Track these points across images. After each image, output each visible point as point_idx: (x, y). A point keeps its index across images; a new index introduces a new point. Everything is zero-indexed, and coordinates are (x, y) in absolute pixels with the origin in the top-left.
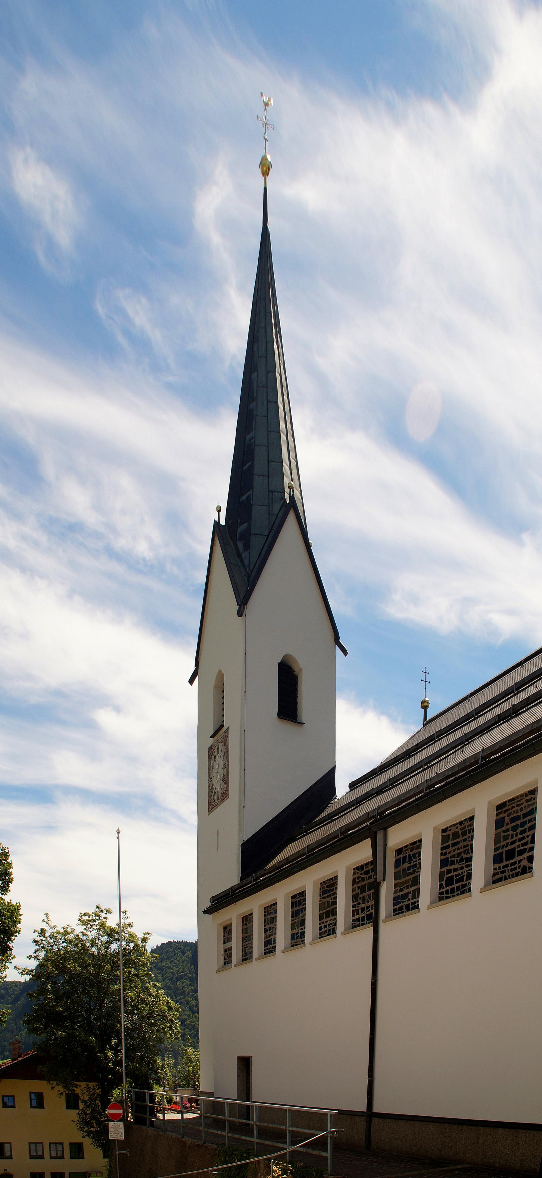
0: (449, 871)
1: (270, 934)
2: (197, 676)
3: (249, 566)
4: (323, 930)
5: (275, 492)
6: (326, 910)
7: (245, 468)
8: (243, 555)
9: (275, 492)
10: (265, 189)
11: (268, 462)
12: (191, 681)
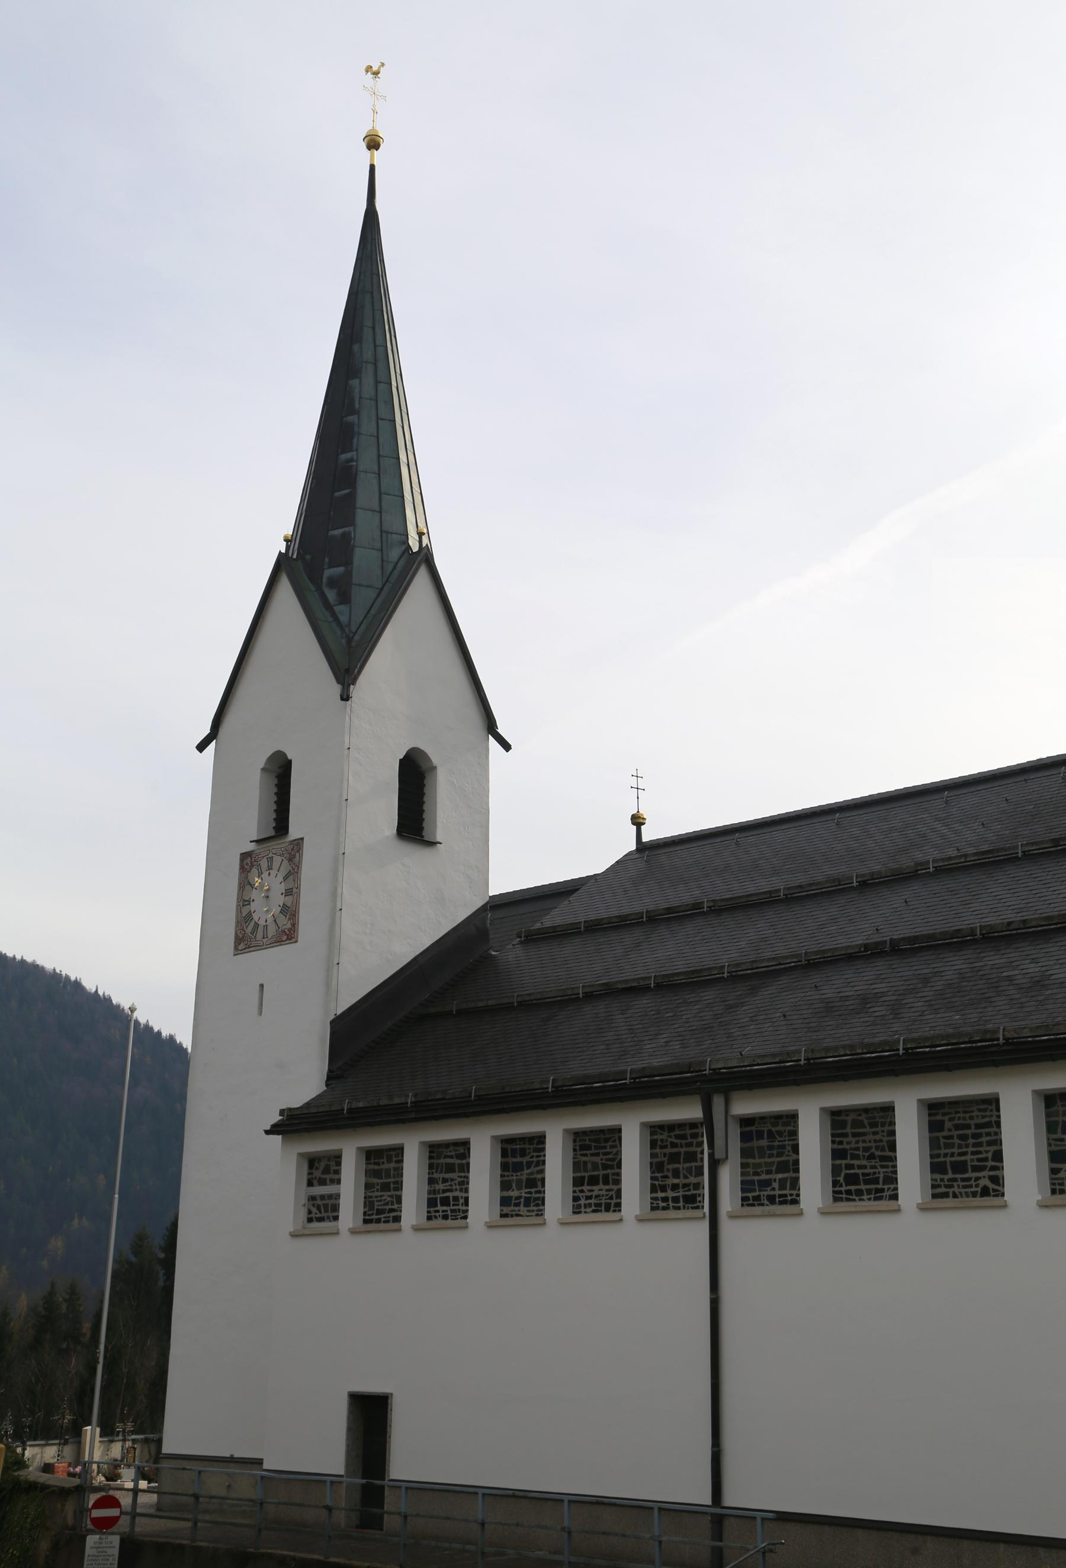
1: (445, 1188)
2: (214, 743)
3: (349, 625)
4: (582, 1202)
6: (589, 1174)
7: (337, 494)
9: (391, 533)
10: (372, 168)
11: (380, 494)
12: (201, 747)
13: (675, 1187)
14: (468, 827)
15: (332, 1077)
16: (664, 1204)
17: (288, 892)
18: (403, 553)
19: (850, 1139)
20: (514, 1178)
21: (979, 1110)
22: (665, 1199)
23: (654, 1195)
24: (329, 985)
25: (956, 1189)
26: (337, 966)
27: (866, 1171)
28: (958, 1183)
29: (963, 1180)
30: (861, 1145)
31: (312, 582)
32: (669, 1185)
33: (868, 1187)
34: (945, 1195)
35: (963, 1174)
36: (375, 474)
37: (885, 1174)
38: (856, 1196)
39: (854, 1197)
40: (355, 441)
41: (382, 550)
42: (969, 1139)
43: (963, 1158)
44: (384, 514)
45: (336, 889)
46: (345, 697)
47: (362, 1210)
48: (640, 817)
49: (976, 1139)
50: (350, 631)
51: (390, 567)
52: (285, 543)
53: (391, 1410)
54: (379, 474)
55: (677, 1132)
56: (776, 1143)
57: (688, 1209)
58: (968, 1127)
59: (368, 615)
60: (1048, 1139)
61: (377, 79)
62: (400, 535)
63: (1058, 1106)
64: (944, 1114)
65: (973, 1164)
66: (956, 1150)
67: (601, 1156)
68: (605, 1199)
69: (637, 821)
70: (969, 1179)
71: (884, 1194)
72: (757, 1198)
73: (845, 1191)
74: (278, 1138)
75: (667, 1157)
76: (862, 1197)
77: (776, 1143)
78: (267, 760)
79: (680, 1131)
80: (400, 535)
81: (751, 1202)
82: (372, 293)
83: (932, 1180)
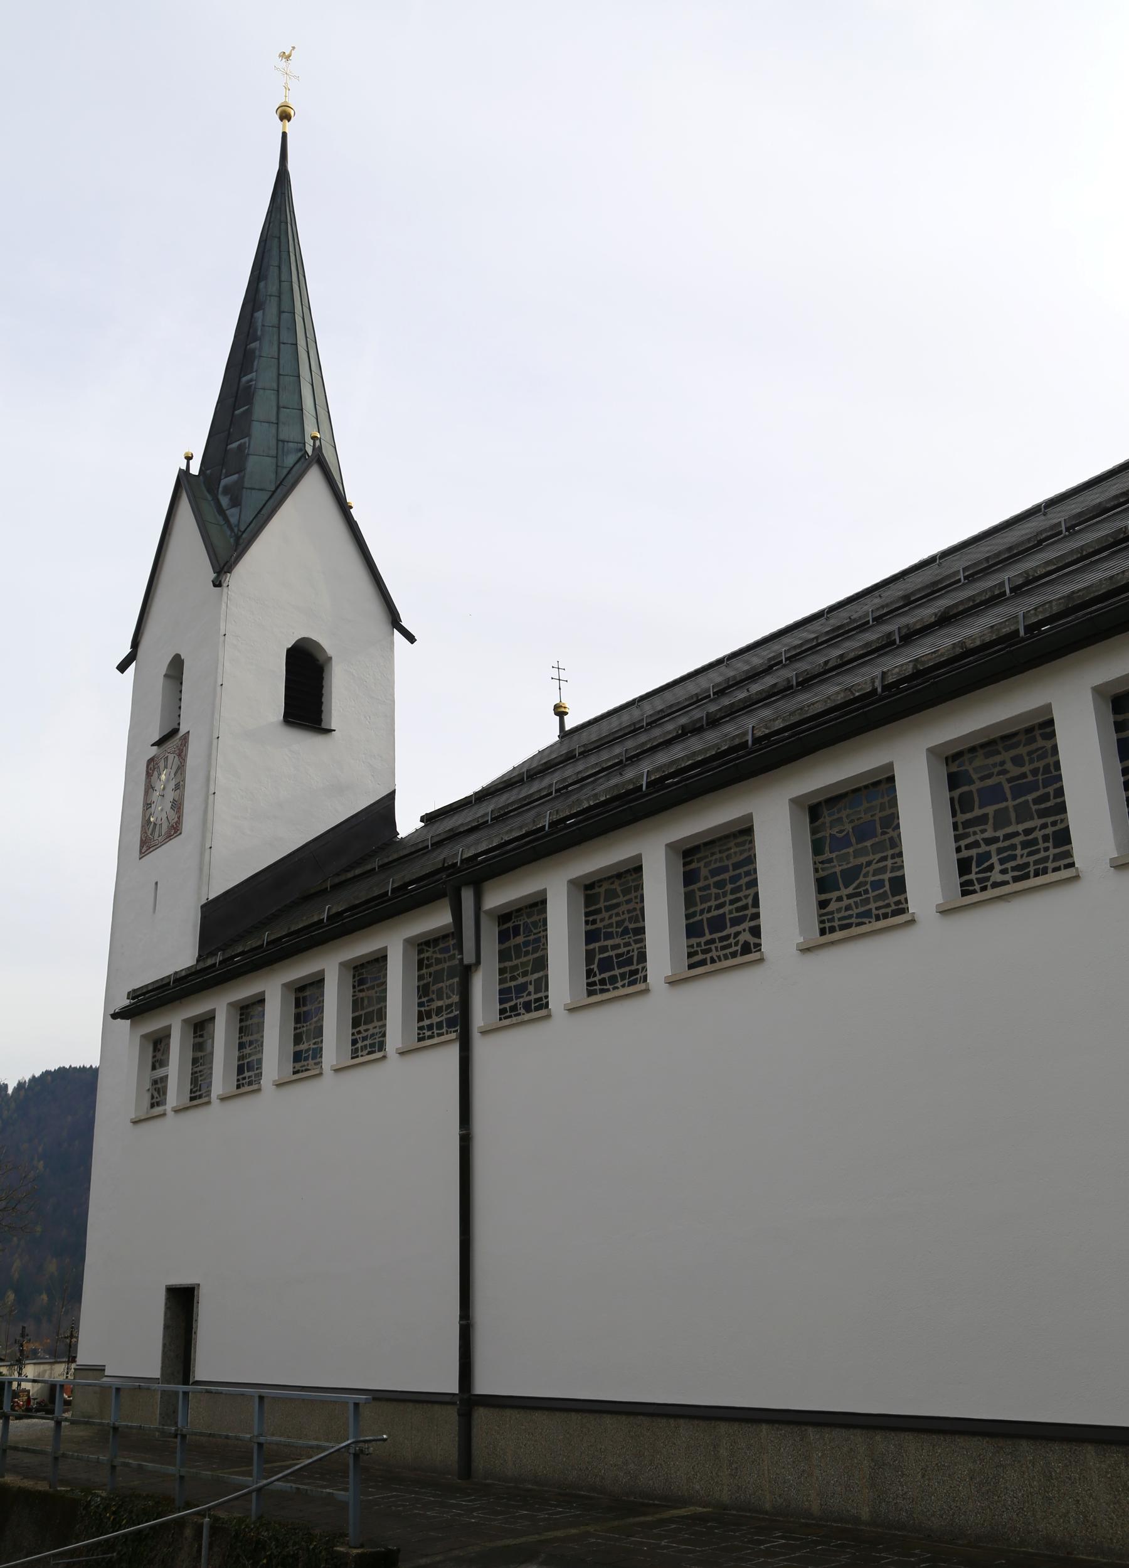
0: (603, 949)
2: (134, 664)
3: (238, 525)
4: (359, 1045)
5: (288, 442)
7: (237, 412)
8: (228, 512)
9: (288, 442)
10: (284, 135)
11: (278, 408)
12: (122, 667)
13: (439, 1011)
14: (370, 717)
15: (198, 961)
16: (429, 1033)
17: (177, 787)
18: (300, 459)
19: (605, 915)
20: (305, 1029)
21: (737, 845)
22: (430, 1027)
23: (421, 1024)
24: (203, 871)
25: (714, 954)
26: (209, 850)
27: (619, 951)
28: (716, 945)
29: (722, 939)
30: (614, 919)
31: (209, 491)
32: (434, 1009)
33: (622, 970)
34: (702, 963)
35: (721, 932)
36: (274, 390)
37: (640, 950)
38: (610, 985)
39: (608, 987)
40: (256, 363)
41: (277, 457)
42: (726, 884)
43: (721, 911)
44: (280, 425)
45: (209, 772)
46: (217, 584)
47: (188, 1087)
48: (561, 706)
49: (734, 884)
50: (239, 530)
51: (285, 472)
52: (186, 461)
53: (198, 1303)
54: (278, 391)
55: (441, 946)
56: (532, 937)
57: (451, 1033)
58: (725, 869)
59: (259, 515)
60: (815, 863)
61: (289, 62)
62: (297, 443)
63: (825, 817)
64: (699, 860)
65: (732, 916)
66: (713, 903)
67: (376, 989)
68: (379, 1037)
69: (560, 712)
70: (728, 937)
71: (638, 976)
72: (514, 1008)
73: (599, 980)
74: (127, 1023)
75: (432, 978)
76: (616, 985)
77: (532, 937)
78: (169, 665)
79: (444, 943)
80: (297, 443)
81: (508, 1014)
82: (279, 238)
83: (688, 947)
